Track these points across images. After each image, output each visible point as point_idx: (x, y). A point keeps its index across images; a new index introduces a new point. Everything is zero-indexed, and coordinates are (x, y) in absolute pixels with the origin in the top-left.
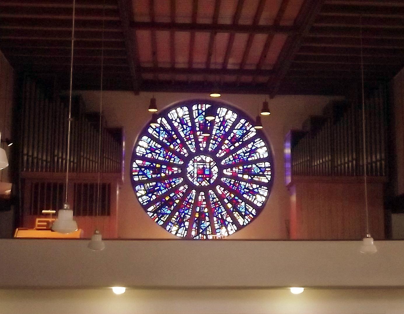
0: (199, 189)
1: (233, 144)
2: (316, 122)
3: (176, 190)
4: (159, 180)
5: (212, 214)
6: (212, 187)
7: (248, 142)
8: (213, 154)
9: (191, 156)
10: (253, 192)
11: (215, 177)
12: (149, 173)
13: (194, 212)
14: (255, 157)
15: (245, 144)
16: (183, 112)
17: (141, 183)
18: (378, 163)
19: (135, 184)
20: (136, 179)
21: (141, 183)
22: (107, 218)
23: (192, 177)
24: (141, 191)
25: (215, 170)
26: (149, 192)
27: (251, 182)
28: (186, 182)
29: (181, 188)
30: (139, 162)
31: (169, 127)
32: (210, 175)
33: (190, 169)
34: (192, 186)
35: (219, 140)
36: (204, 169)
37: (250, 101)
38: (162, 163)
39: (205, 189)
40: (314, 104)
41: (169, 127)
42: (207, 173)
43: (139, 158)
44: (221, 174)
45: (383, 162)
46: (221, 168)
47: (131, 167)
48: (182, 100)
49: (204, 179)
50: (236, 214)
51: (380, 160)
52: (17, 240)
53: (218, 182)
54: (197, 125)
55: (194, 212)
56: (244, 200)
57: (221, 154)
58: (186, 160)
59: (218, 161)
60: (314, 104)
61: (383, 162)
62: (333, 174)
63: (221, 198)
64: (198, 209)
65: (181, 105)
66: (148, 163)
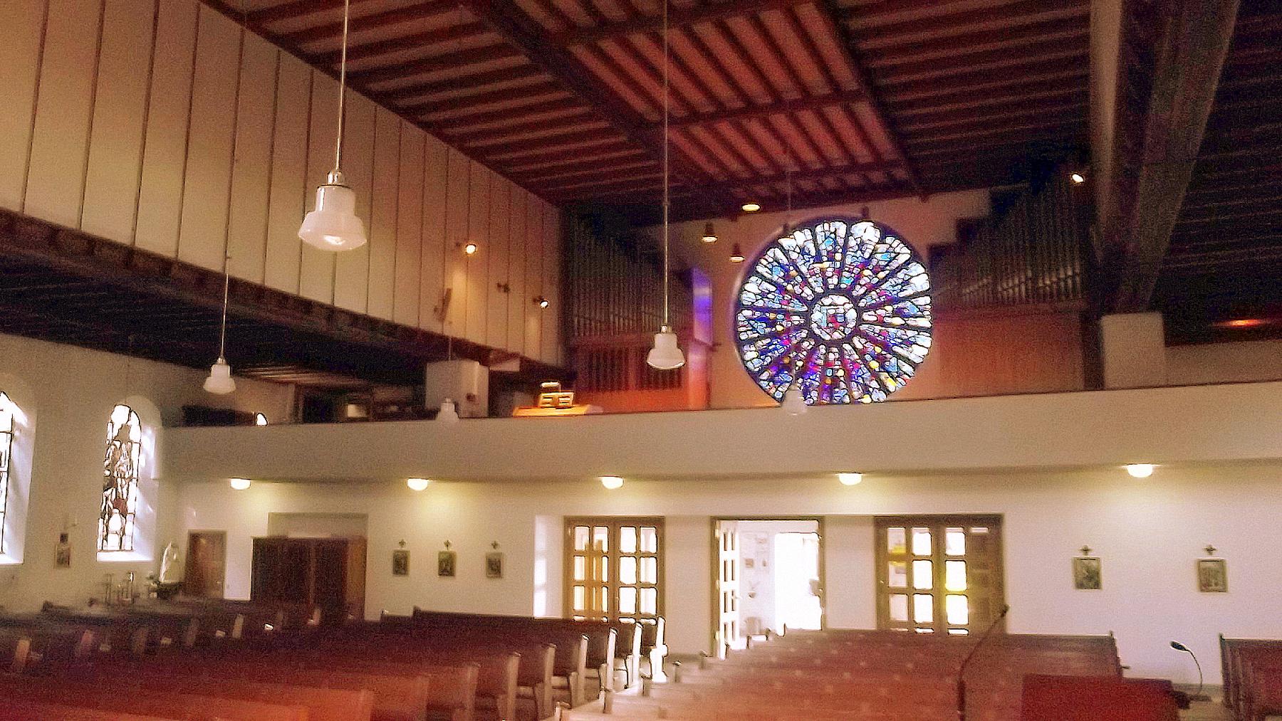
0: (829, 345)
1: (876, 273)
2: (966, 229)
3: (798, 348)
4: (775, 335)
5: (803, 373)
6: (848, 340)
7: (899, 269)
8: (847, 292)
9: (818, 297)
10: (908, 343)
11: (852, 325)
12: (761, 327)
13: (823, 377)
14: (909, 291)
15: (893, 274)
16: (801, 237)
17: (751, 342)
18: (1070, 282)
19: (740, 344)
20: (743, 337)
21: (751, 342)
22: (676, 391)
23: (819, 327)
24: (751, 354)
25: (852, 314)
26: (763, 353)
27: (905, 327)
28: (811, 335)
29: (805, 344)
30: (748, 313)
31: (785, 261)
32: (845, 323)
33: (816, 316)
34: (819, 341)
35: (856, 271)
36: (835, 315)
37: (886, 208)
38: (777, 311)
39: (838, 343)
40: (973, 202)
41: (785, 261)
42: (840, 319)
43: (748, 308)
44: (860, 320)
45: (1078, 279)
46: (860, 311)
47: (736, 321)
48: (803, 219)
49: (835, 329)
50: (884, 376)
51: (1073, 277)
52: (520, 421)
53: (856, 332)
54: (824, 253)
55: (823, 377)
56: (895, 354)
57: (859, 291)
58: (811, 304)
59: (855, 301)
60: (973, 202)
61: (1078, 279)
62: (997, 306)
63: (862, 353)
64: (829, 373)
65: (801, 227)
66: (758, 314)
